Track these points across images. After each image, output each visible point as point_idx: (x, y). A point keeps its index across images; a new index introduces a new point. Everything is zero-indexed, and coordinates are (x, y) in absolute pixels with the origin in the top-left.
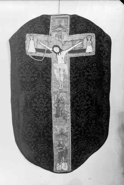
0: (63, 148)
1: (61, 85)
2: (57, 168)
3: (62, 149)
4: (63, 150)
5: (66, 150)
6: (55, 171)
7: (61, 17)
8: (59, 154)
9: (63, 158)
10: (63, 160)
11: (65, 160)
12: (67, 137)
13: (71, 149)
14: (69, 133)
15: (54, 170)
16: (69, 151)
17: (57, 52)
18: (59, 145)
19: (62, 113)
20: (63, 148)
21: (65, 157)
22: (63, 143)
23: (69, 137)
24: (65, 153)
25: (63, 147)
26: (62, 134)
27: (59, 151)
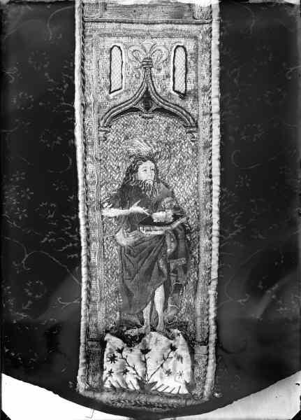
0: (158, 216)
1: (186, 116)
2: (108, 365)
3: (148, 221)
4: (158, 231)
5: (186, 236)
6: (91, 389)
7: (87, 289)
8: (123, 264)
9: (159, 294)
10: (159, 307)
11: (171, 313)
12: (192, 126)
13: (216, 227)
14: (203, 99)
15: (81, 386)
16: (204, 241)
17: (183, 49)
18: (128, 191)
19: (176, 217)
20: (158, 216)
21: (172, 291)
22: (157, 180)
23: (203, 133)
24: (175, 256)
25: (156, 206)
26: (147, 98)
27: (125, 239)
